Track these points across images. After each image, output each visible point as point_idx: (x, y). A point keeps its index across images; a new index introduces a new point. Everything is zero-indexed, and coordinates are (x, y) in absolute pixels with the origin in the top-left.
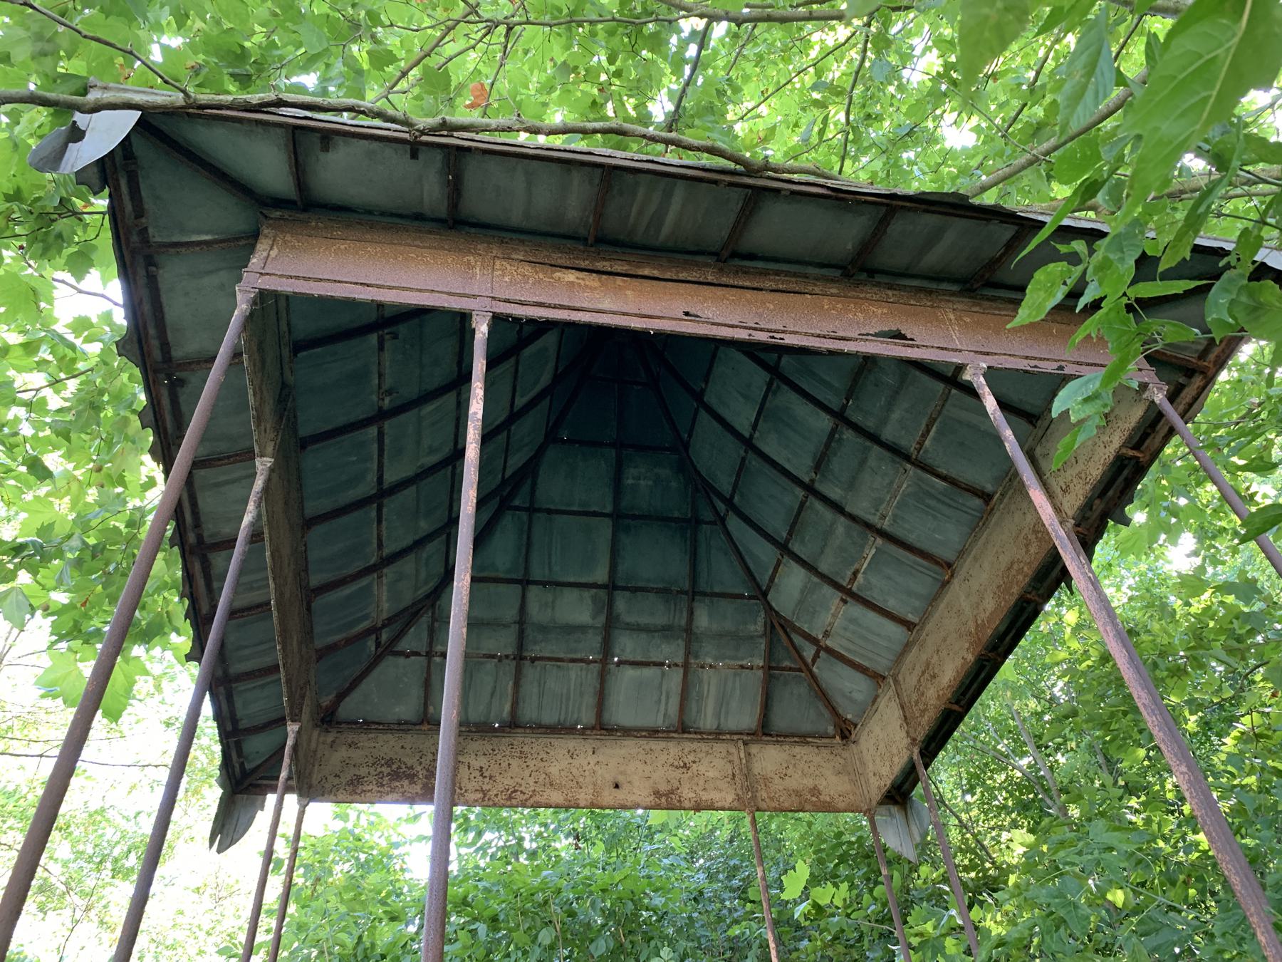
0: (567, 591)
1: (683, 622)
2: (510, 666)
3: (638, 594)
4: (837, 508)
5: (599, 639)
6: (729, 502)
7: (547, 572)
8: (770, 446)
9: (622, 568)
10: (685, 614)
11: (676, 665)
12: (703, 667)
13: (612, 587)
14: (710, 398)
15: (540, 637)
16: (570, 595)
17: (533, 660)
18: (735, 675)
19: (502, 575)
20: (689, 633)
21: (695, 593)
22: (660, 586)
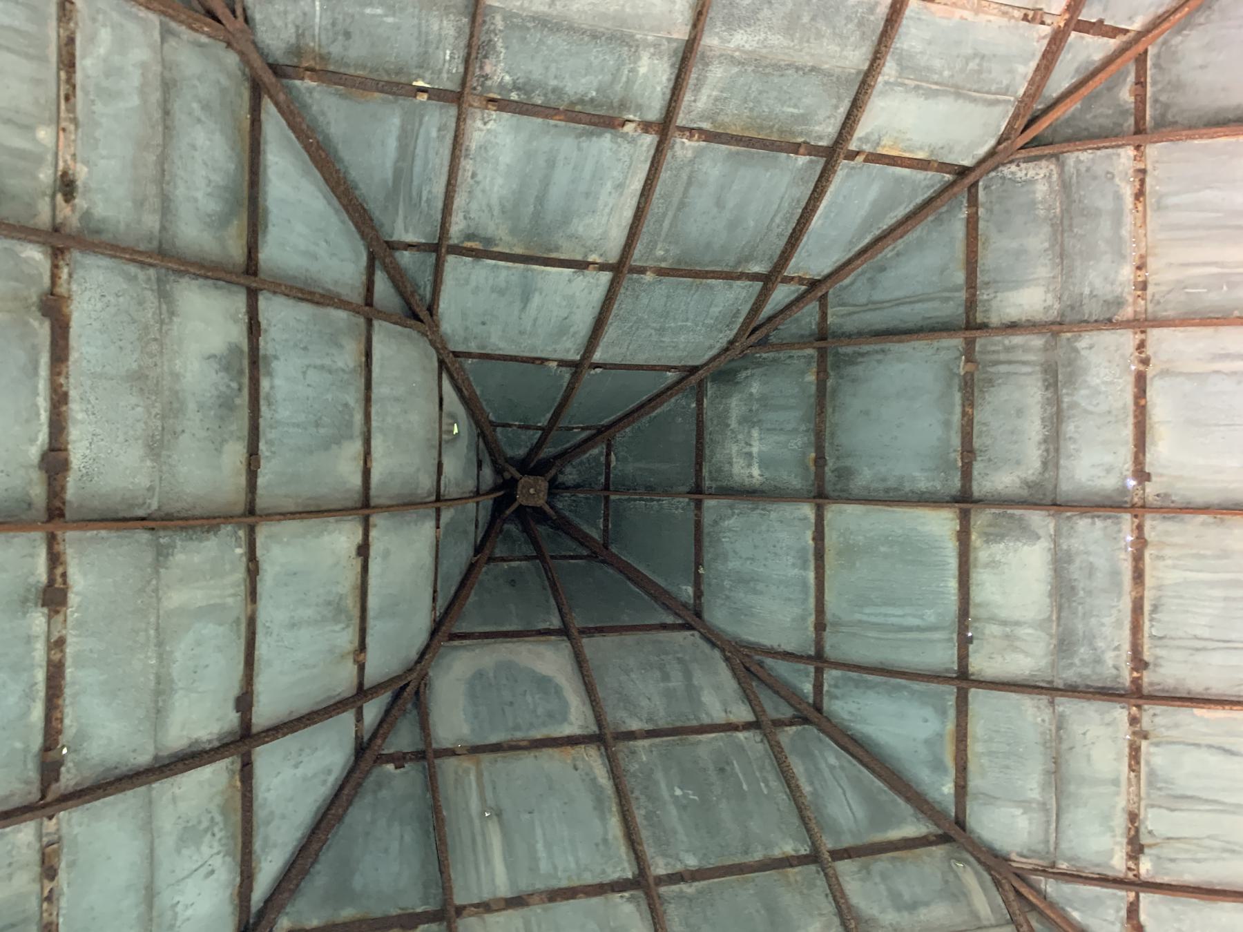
0: (977, 595)
1: (1037, 341)
2: (1157, 717)
3: (977, 443)
4: (687, 58)
5: (1083, 524)
6: (768, 280)
7: (937, 635)
8: (606, 226)
9: (923, 482)
10: (1017, 340)
11: (1141, 346)
12: (1144, 286)
13: (964, 501)
14: (570, 349)
15: (1083, 651)
16: (986, 587)
17: (1139, 663)
18: (1159, 208)
19: (950, 726)
20: (1061, 326)
21: (971, 325)
22: (957, 397)
